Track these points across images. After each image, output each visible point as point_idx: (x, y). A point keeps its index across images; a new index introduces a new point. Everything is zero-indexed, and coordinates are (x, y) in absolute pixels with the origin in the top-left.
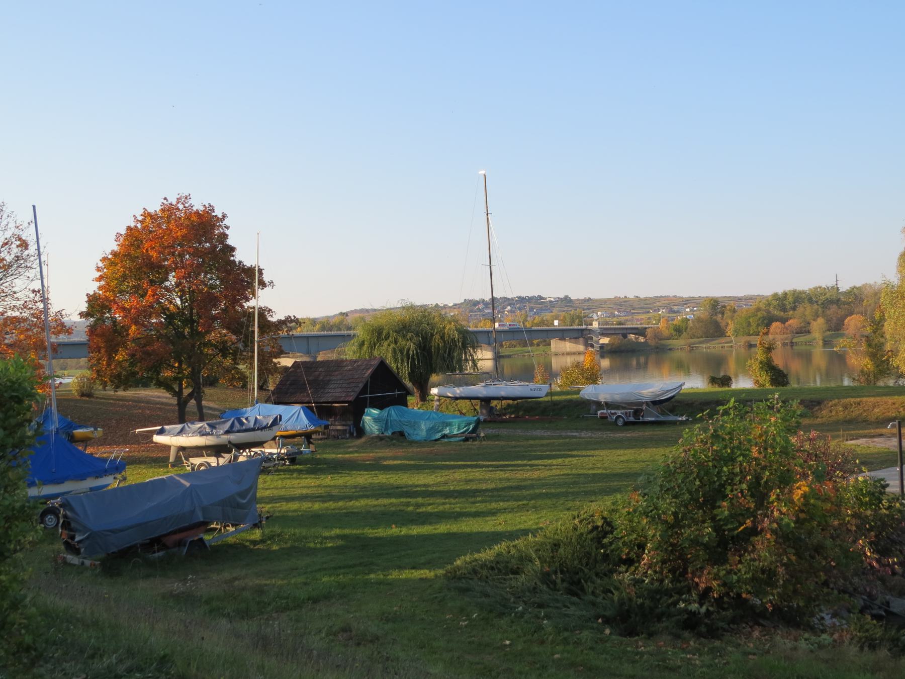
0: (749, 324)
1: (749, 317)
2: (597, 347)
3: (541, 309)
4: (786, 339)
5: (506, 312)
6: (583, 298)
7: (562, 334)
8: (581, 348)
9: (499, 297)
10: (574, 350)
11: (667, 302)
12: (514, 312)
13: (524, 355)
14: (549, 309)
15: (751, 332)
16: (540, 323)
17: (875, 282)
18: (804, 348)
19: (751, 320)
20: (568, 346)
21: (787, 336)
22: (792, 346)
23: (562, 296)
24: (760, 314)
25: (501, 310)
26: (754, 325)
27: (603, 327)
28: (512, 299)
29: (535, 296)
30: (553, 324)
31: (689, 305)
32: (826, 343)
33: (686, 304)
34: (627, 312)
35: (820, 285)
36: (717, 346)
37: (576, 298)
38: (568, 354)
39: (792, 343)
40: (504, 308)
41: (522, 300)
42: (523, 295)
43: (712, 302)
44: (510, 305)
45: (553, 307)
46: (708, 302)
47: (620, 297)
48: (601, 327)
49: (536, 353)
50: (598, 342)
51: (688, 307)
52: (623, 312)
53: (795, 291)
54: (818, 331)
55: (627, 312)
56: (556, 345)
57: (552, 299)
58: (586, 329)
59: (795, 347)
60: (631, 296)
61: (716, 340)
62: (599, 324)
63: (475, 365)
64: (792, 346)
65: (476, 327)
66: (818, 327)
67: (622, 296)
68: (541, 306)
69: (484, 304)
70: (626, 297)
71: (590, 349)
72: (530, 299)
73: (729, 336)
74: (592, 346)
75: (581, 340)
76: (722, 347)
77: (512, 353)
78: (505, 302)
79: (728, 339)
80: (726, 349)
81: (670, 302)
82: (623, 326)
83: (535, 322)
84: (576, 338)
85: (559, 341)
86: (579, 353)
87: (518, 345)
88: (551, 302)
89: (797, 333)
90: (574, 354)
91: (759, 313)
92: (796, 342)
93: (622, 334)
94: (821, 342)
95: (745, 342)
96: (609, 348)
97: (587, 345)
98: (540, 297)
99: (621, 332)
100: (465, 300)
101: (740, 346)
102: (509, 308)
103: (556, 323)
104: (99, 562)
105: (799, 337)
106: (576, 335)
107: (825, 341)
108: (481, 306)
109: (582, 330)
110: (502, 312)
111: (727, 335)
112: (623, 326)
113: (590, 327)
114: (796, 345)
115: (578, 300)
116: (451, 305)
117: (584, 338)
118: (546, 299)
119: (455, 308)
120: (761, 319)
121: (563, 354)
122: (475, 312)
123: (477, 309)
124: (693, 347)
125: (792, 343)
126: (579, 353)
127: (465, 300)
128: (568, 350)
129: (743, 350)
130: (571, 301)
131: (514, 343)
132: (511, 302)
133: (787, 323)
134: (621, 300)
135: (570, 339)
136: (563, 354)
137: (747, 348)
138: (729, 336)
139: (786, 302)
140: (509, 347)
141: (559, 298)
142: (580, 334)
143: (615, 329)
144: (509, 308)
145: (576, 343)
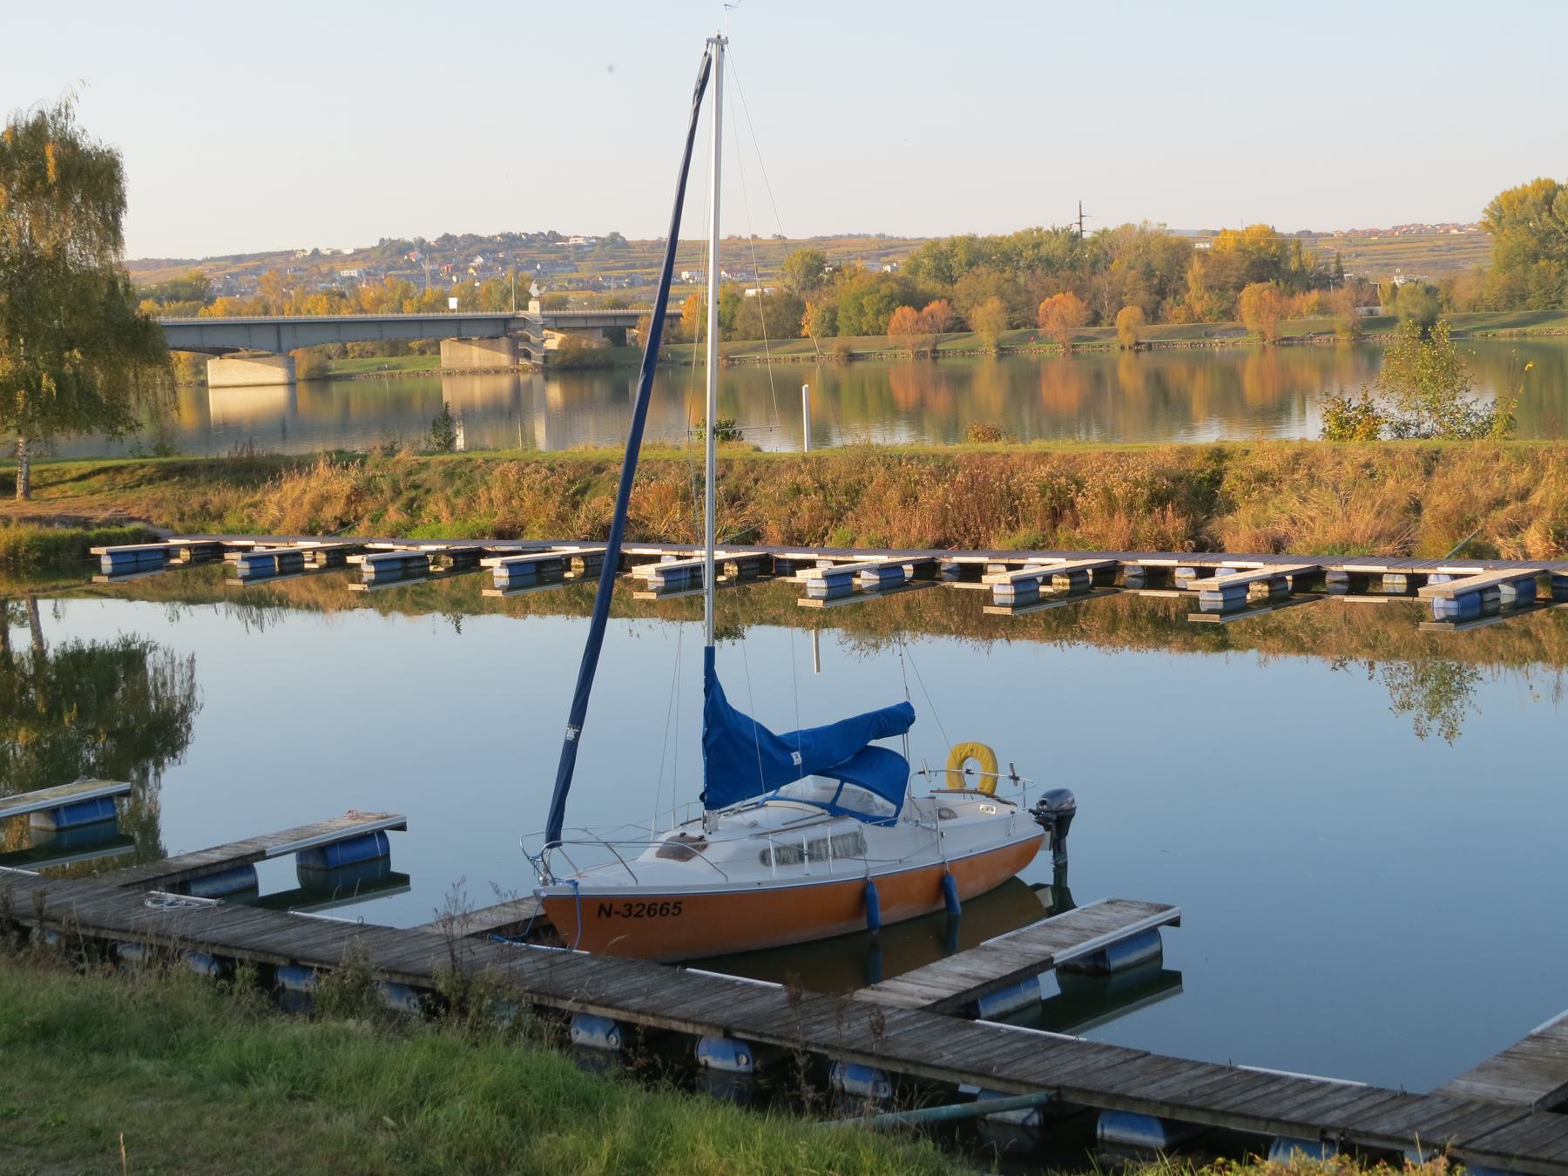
0: (861, 311)
1: (863, 294)
2: (537, 357)
3: (554, 264)
4: (924, 344)
5: (471, 271)
6: (655, 239)
7: (461, 329)
8: (504, 359)
9: (459, 235)
10: (488, 364)
11: (844, 249)
12: (490, 269)
13: (380, 376)
14: (571, 264)
15: (865, 328)
16: (436, 301)
17: (1146, 222)
18: (960, 361)
19: (864, 301)
20: (476, 354)
21: (924, 336)
22: (935, 359)
23: (604, 234)
24: (885, 289)
25: (461, 266)
26: (870, 311)
27: (551, 312)
28: (491, 240)
29: (543, 234)
30: (446, 304)
31: (891, 258)
32: (1003, 352)
33: (887, 255)
34: (749, 273)
35: (1040, 226)
36: (782, 357)
37: (640, 239)
38: (474, 372)
39: (935, 351)
40: (469, 259)
41: (511, 241)
42: (516, 231)
43: (808, 259)
44: (482, 253)
45: (582, 259)
46: (799, 260)
47: (740, 238)
48: (546, 312)
49: (407, 371)
50: (538, 347)
51: (890, 263)
52: (739, 271)
53: (971, 239)
54: (985, 328)
55: (749, 273)
56: (452, 353)
57: (580, 241)
58: (514, 318)
59: (940, 361)
60: (766, 234)
61: (788, 343)
62: (542, 309)
63: (201, 402)
64: (935, 359)
65: (400, 309)
66: (987, 316)
67: (746, 235)
68: (553, 256)
69: (422, 251)
70: (754, 237)
71: (523, 362)
72: (529, 241)
73: (807, 336)
74: (527, 355)
75: (504, 341)
76: (793, 360)
77: (358, 370)
78: (472, 245)
79: (802, 344)
80: (801, 363)
81: (851, 249)
82: (626, 311)
83: (426, 299)
84: (492, 338)
85: (457, 343)
86: (497, 372)
87: (379, 352)
88: (578, 247)
89: (949, 330)
90: (486, 372)
91: (883, 286)
92: (944, 351)
93: (604, 328)
94: (993, 352)
95: (840, 350)
96: (558, 360)
97: (517, 353)
98: (555, 236)
99: (603, 323)
100: (382, 241)
101: (830, 358)
102: (479, 260)
103: (453, 303)
104: (743, 1064)
105: (956, 338)
106: (490, 330)
107: (1002, 349)
108: (415, 256)
109: (506, 320)
110: (462, 270)
111: (803, 334)
112: (626, 311)
113: (522, 314)
114: (944, 357)
115: (643, 243)
116: (349, 251)
117: (510, 337)
118: (567, 239)
119: (355, 260)
120: (886, 301)
121: (463, 373)
122: (401, 269)
123: (406, 262)
124: (734, 360)
125: (935, 351)
126: (497, 372)
127: (382, 241)
128: (476, 363)
129: (834, 366)
130: (625, 244)
131: (369, 346)
132: (484, 246)
133: (926, 309)
134: (741, 245)
135: (480, 338)
136: (463, 373)
137: (842, 363)
138: (807, 336)
139: (953, 262)
140: (360, 356)
141: (597, 238)
142: (501, 329)
143: (586, 318)
144: (479, 260)
145: (493, 349)
